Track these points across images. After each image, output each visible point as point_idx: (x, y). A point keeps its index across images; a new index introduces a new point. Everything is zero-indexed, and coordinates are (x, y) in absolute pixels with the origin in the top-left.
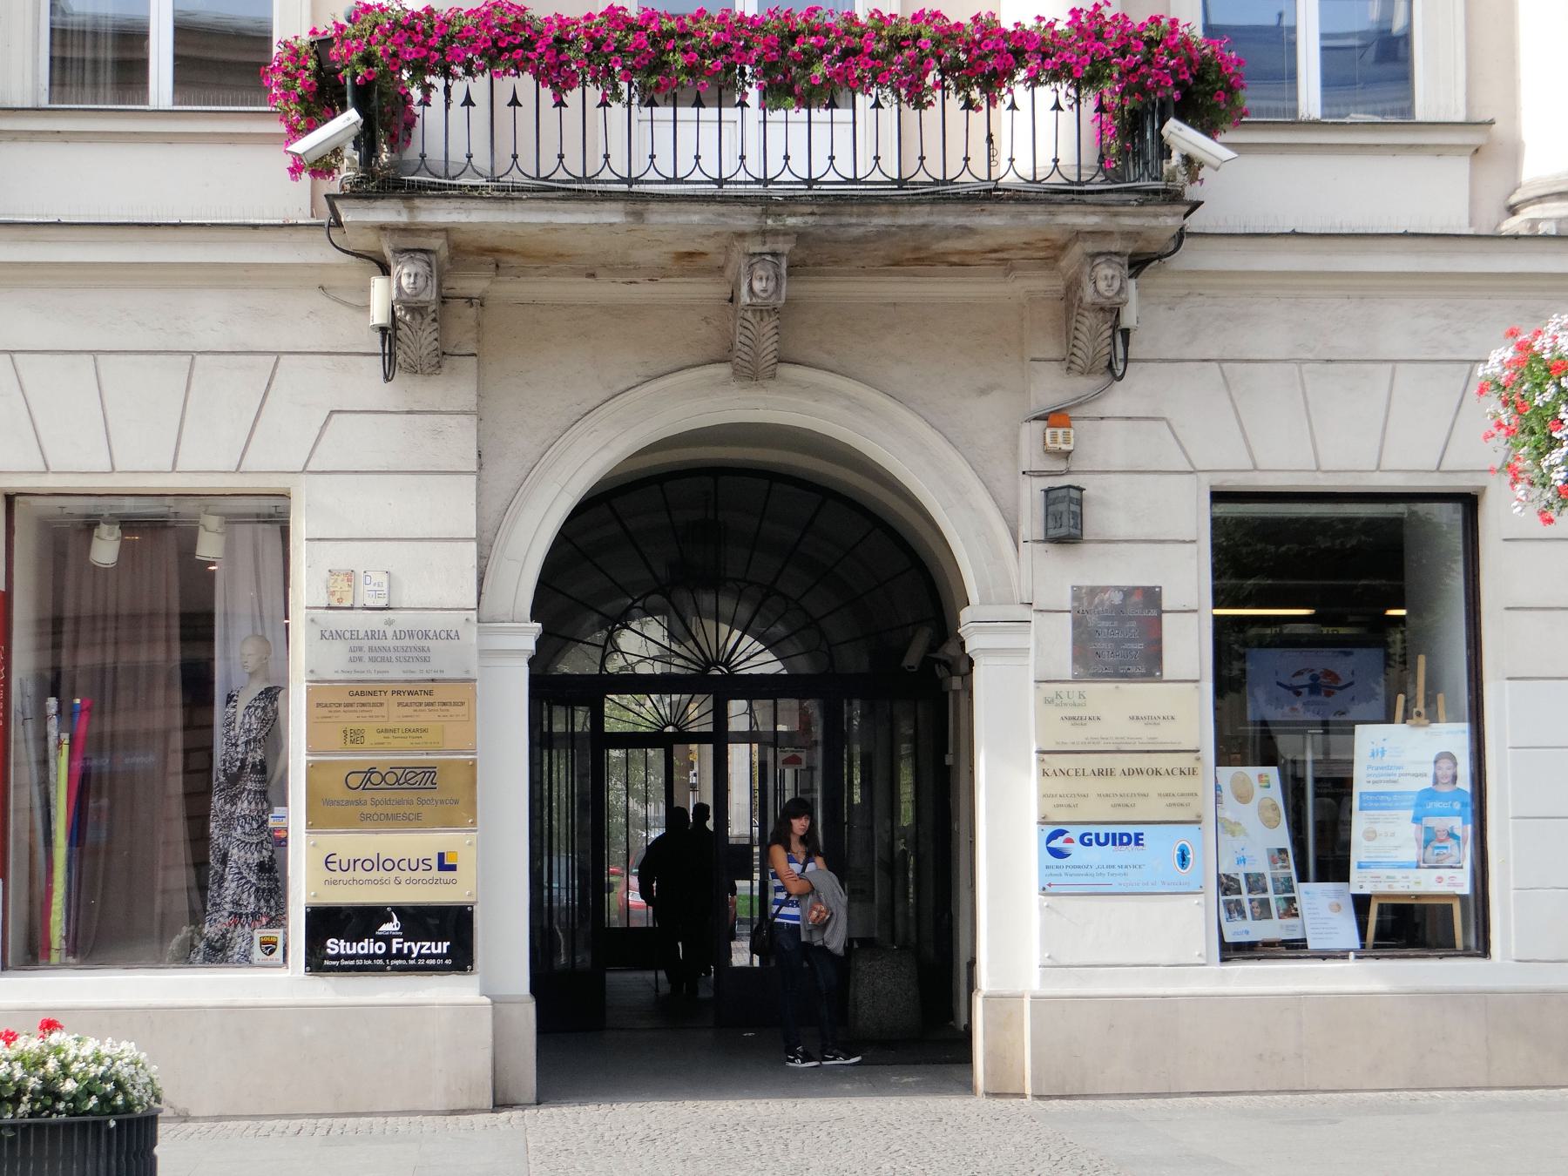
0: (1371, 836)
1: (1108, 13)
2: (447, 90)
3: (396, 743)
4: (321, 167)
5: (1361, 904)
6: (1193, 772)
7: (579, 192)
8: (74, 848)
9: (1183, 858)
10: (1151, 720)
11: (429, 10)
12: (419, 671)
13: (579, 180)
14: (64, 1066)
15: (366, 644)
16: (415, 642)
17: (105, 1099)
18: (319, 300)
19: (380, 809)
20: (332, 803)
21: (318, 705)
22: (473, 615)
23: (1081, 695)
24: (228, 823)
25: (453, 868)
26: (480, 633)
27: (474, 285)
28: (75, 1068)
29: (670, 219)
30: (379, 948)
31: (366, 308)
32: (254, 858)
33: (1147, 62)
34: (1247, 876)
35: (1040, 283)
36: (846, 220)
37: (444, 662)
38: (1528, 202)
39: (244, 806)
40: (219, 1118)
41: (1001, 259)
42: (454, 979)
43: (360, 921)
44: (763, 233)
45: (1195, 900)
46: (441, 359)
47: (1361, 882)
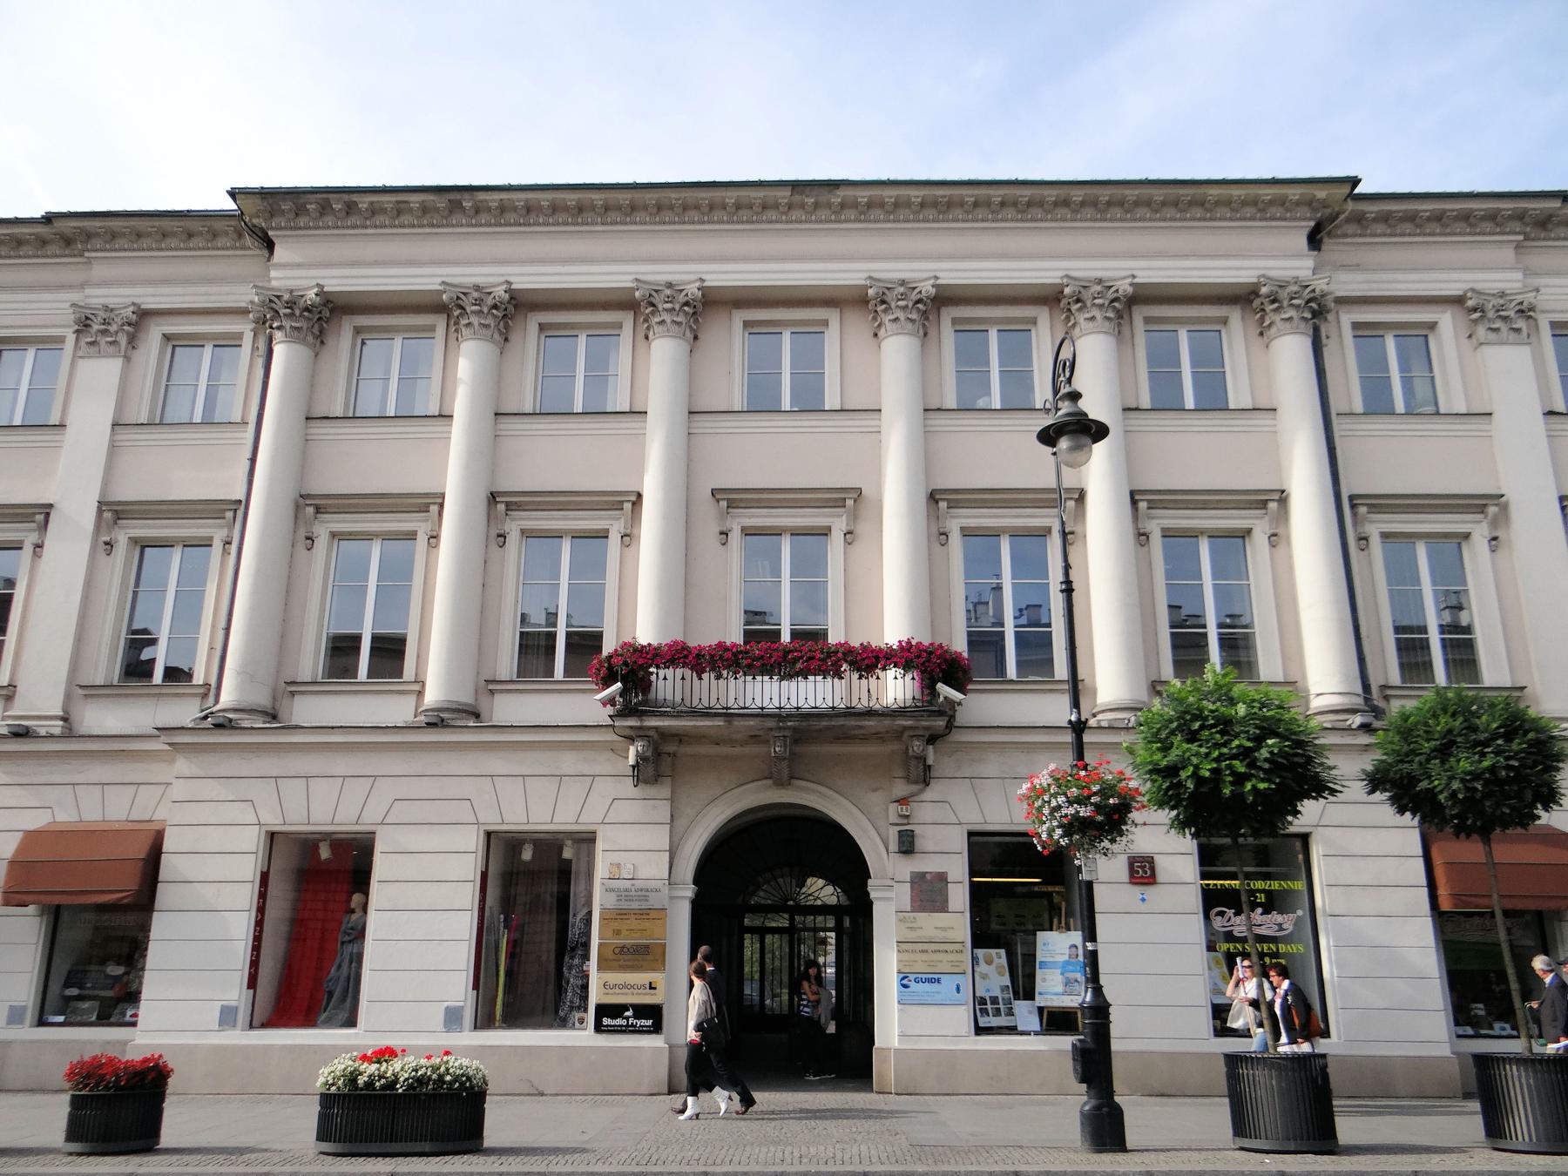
0: (1044, 980)
1: (914, 643)
2: (657, 674)
3: (634, 935)
4: (610, 701)
5: (1041, 1010)
6: (961, 951)
7: (707, 713)
8: (112, 1020)
9: (958, 990)
10: (944, 929)
11: (649, 644)
12: (644, 905)
13: (707, 708)
14: (447, 1069)
15: (623, 894)
16: (643, 893)
17: (462, 1084)
18: (611, 754)
19: (627, 963)
20: (607, 960)
21: (602, 919)
22: (667, 882)
23: (914, 918)
24: (570, 968)
25: (655, 988)
26: (670, 890)
27: (671, 748)
28: (451, 1071)
29: (742, 723)
30: (624, 1022)
31: (627, 758)
32: (580, 982)
33: (929, 661)
34: (990, 997)
35: (894, 747)
36: (811, 723)
37: (655, 901)
38: (1099, 712)
39: (576, 961)
40: (557, 1095)
41: (879, 737)
42: (654, 1036)
43: (614, 1010)
44: (780, 728)
45: (964, 1007)
46: (655, 779)
47: (1040, 1001)
